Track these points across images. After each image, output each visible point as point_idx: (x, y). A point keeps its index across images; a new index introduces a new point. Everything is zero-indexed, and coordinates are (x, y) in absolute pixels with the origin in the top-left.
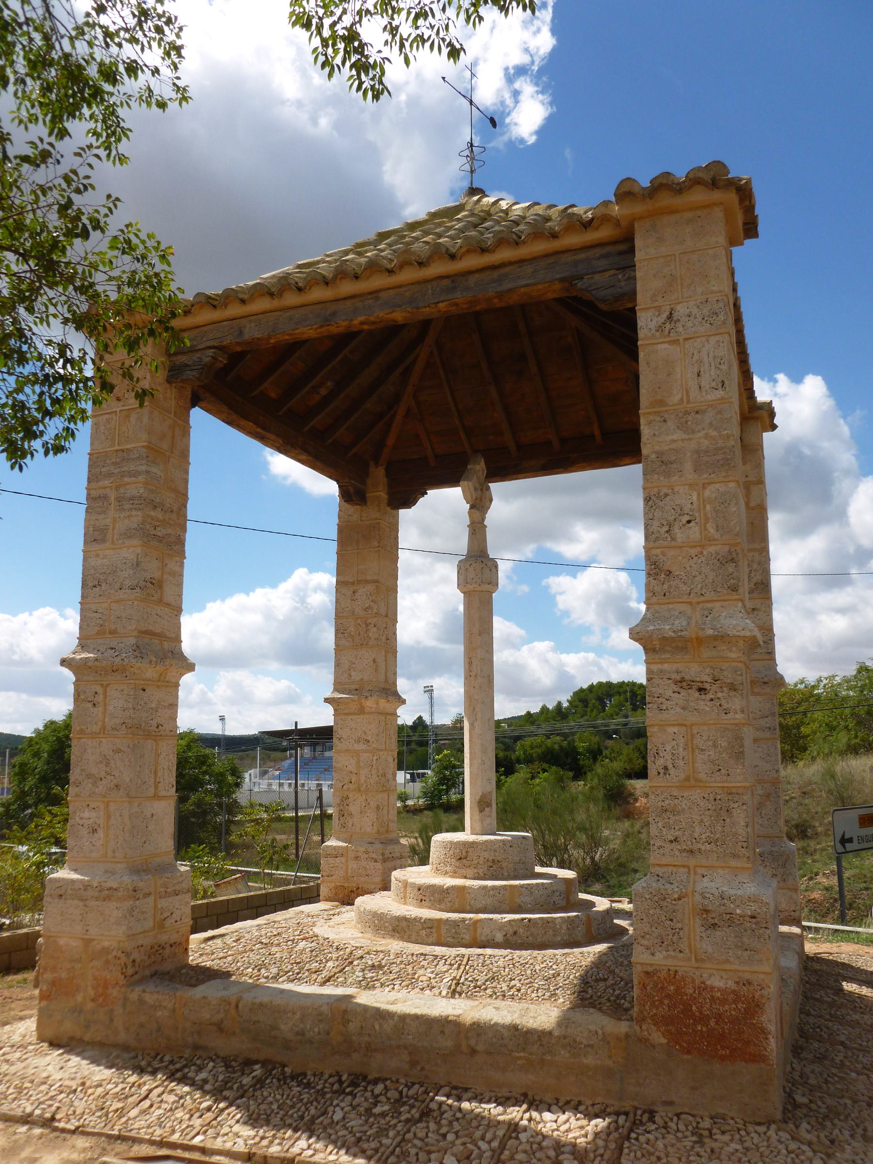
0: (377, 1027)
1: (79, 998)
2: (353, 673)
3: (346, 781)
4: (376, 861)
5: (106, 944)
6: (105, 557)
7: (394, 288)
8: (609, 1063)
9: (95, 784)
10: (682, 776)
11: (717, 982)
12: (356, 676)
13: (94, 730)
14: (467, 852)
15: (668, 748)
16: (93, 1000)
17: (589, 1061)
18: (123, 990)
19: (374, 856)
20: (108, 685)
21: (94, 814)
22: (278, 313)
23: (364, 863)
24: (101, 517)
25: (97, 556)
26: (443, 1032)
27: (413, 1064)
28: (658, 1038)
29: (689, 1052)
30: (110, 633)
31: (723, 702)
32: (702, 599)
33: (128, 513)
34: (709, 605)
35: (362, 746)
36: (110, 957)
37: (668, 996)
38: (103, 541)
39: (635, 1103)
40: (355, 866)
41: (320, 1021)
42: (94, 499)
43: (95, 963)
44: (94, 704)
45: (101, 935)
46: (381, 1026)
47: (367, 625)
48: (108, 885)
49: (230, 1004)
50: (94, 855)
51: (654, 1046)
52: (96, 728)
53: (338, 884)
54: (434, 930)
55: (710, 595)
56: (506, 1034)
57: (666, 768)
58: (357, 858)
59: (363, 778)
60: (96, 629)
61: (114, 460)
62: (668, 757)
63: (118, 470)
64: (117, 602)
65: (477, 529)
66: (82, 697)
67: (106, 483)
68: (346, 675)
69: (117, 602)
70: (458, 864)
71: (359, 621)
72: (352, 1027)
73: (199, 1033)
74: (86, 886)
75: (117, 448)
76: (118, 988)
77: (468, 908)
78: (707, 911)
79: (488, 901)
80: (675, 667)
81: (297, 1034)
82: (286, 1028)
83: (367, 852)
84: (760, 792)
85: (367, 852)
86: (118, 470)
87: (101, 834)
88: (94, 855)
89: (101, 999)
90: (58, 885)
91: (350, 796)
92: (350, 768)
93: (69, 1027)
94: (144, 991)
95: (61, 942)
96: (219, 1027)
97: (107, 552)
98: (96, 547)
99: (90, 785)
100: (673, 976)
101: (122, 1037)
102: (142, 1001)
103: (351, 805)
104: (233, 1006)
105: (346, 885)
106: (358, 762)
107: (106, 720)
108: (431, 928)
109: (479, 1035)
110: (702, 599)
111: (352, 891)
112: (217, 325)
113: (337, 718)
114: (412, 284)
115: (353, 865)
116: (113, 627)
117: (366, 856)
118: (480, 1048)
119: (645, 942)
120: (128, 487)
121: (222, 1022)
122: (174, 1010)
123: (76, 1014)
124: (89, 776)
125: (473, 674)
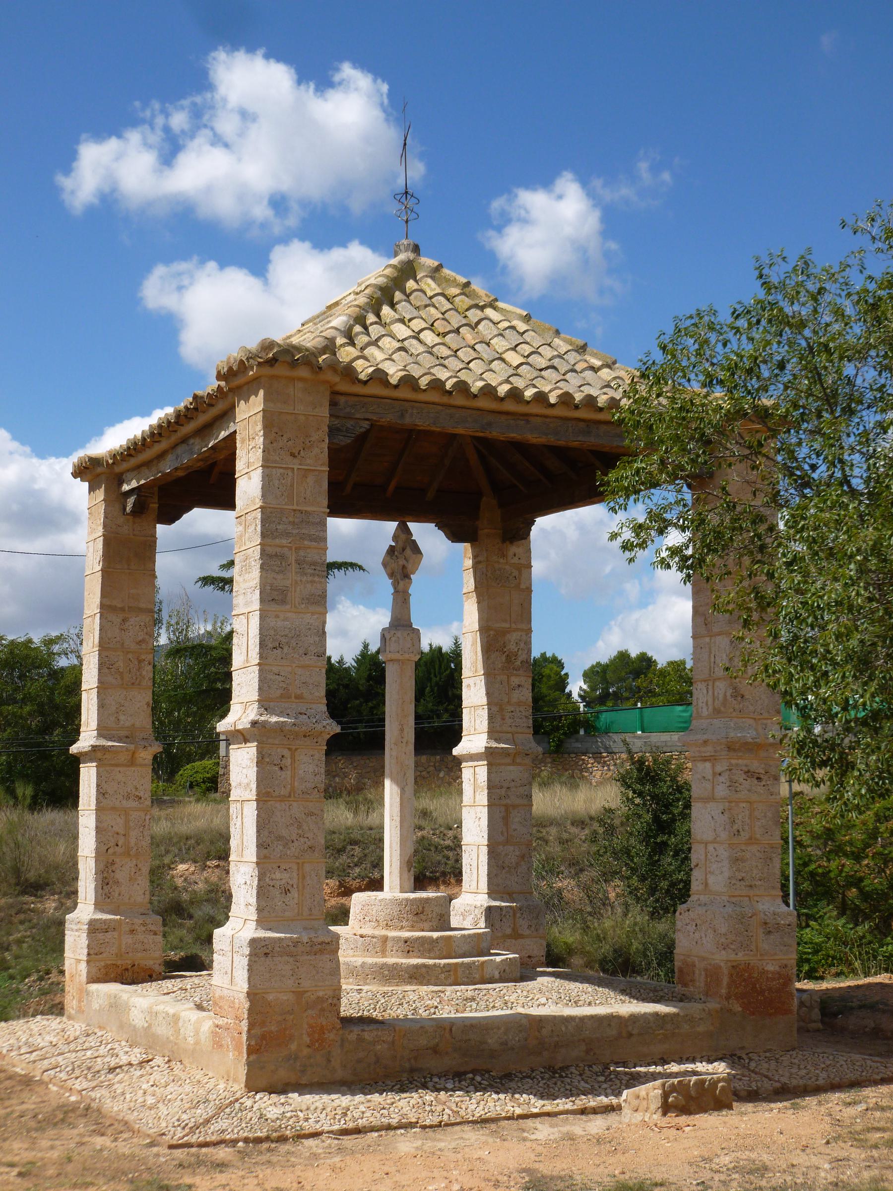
0: (563, 1029)
1: (293, 1047)
2: (122, 718)
3: (112, 844)
4: (155, 934)
5: (321, 994)
6: (286, 619)
7: (541, 416)
8: (712, 1028)
9: (285, 845)
10: (747, 837)
11: (770, 968)
12: (126, 721)
13: (282, 793)
14: (423, 908)
15: (740, 817)
16: (308, 1046)
17: (701, 1029)
18: (341, 1032)
19: (153, 928)
20: (296, 749)
21: (286, 876)
22: (440, 408)
23: (141, 937)
24: (280, 576)
25: (277, 616)
26: (609, 1025)
27: (587, 1052)
28: (737, 1008)
29: (753, 1014)
30: (296, 698)
31: (770, 787)
32: (761, 717)
33: (310, 579)
34: (765, 721)
35: (132, 804)
36: (325, 1005)
37: (744, 980)
38: (283, 602)
39: (724, 1052)
40: (130, 941)
41: (520, 1031)
42: (270, 556)
43: (310, 1012)
44: (281, 768)
45: (316, 986)
46: (567, 1027)
47: (140, 661)
48: (320, 939)
49: (445, 1029)
50: (287, 914)
51: (735, 1014)
52: (284, 792)
53: (109, 962)
54: (452, 973)
55: (766, 715)
56: (651, 1019)
57: (738, 831)
58: (132, 931)
59: (133, 841)
60: (279, 692)
61: (291, 519)
62: (740, 823)
63: (297, 531)
64: (303, 667)
65: (402, 599)
66: (268, 760)
67: (284, 542)
68: (113, 719)
69: (303, 667)
70: (415, 919)
71: (130, 656)
72: (544, 1032)
73: (416, 1058)
74: (296, 943)
75: (295, 507)
76: (335, 1032)
77: (454, 954)
78: (766, 923)
79: (466, 948)
80: (745, 762)
81: (502, 1044)
82: (492, 1041)
83: (144, 924)
84: (517, 853)
85: (144, 924)
86: (297, 531)
87: (294, 893)
88: (287, 914)
89: (317, 1045)
90: (263, 944)
91: (117, 860)
92: (116, 829)
93: (283, 1074)
94: (363, 1031)
95: (270, 997)
96: (435, 1050)
97: (289, 615)
98: (274, 607)
99: (281, 848)
100: (748, 967)
101: (340, 1074)
102: (360, 1040)
103: (118, 871)
104: (447, 1030)
105: (119, 963)
106: (127, 822)
107: (296, 784)
108: (449, 971)
109: (634, 1023)
110: (761, 717)
111: (127, 969)
112: (379, 400)
113: (102, 769)
114: (556, 417)
115: (127, 940)
116: (299, 692)
117: (144, 929)
118: (635, 1032)
119: (732, 947)
120: (308, 551)
121: (437, 1045)
122: (393, 1042)
123: (291, 1062)
124: (279, 838)
125: (404, 740)
